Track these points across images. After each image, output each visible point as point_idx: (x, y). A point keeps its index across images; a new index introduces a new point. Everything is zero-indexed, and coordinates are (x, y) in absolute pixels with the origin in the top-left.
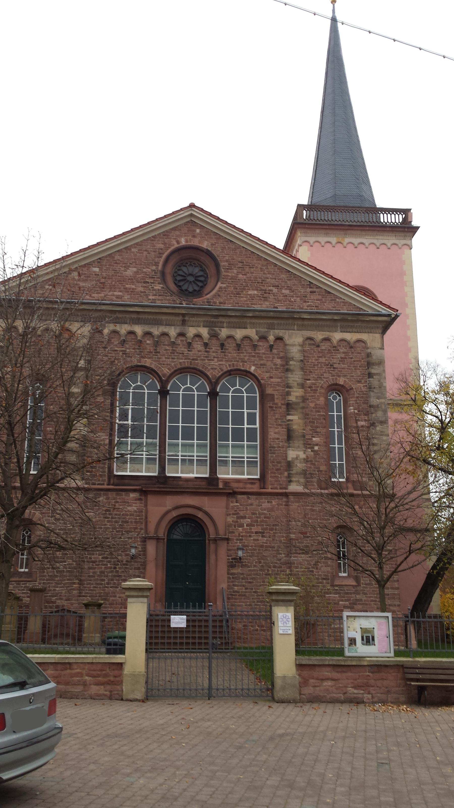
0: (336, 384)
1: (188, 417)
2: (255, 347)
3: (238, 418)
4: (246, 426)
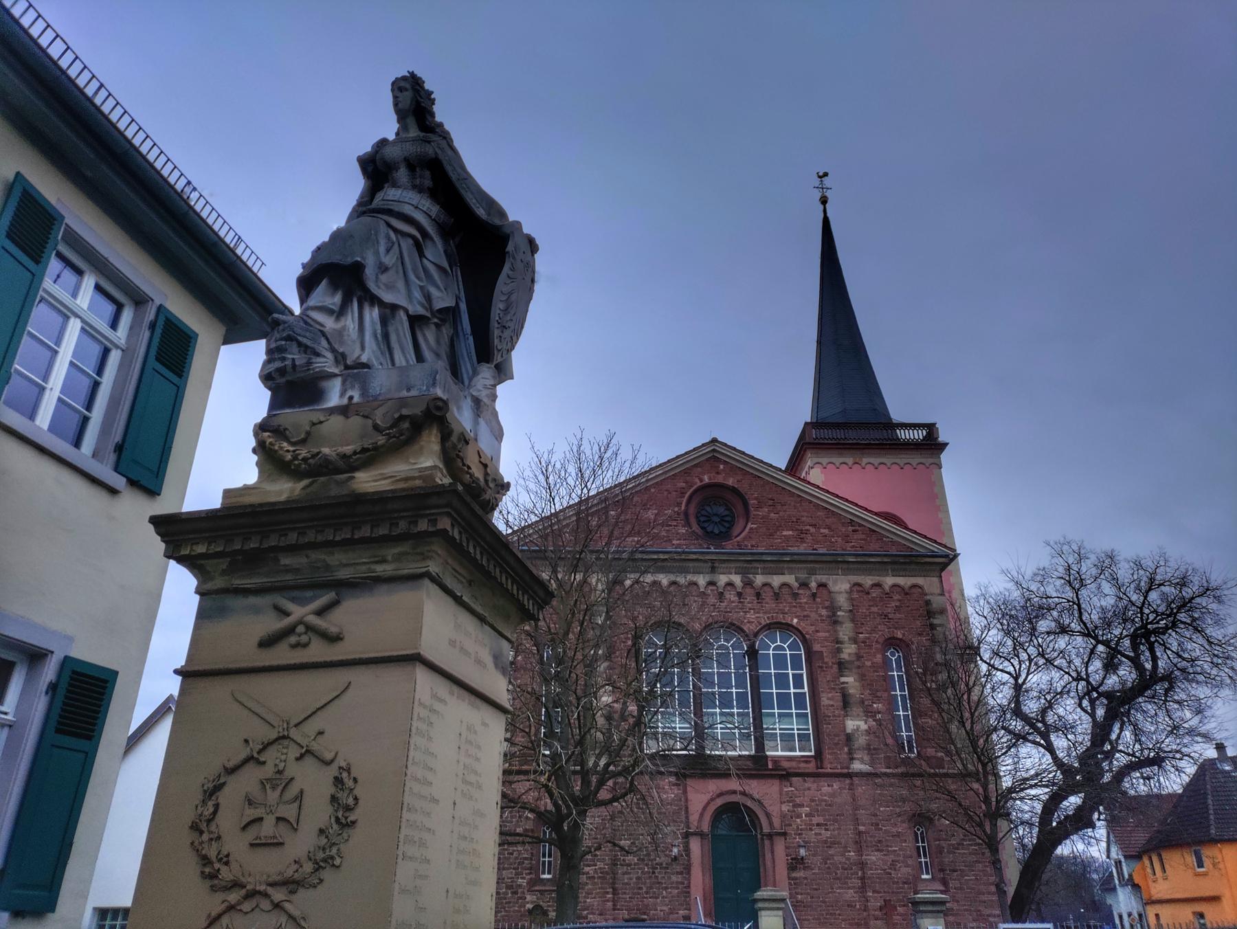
0: (894, 638)
1: (724, 680)
2: (795, 596)
3: (782, 681)
4: (792, 690)
